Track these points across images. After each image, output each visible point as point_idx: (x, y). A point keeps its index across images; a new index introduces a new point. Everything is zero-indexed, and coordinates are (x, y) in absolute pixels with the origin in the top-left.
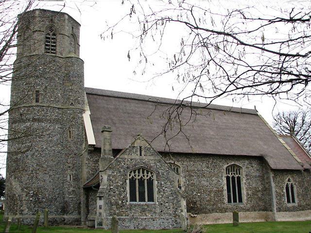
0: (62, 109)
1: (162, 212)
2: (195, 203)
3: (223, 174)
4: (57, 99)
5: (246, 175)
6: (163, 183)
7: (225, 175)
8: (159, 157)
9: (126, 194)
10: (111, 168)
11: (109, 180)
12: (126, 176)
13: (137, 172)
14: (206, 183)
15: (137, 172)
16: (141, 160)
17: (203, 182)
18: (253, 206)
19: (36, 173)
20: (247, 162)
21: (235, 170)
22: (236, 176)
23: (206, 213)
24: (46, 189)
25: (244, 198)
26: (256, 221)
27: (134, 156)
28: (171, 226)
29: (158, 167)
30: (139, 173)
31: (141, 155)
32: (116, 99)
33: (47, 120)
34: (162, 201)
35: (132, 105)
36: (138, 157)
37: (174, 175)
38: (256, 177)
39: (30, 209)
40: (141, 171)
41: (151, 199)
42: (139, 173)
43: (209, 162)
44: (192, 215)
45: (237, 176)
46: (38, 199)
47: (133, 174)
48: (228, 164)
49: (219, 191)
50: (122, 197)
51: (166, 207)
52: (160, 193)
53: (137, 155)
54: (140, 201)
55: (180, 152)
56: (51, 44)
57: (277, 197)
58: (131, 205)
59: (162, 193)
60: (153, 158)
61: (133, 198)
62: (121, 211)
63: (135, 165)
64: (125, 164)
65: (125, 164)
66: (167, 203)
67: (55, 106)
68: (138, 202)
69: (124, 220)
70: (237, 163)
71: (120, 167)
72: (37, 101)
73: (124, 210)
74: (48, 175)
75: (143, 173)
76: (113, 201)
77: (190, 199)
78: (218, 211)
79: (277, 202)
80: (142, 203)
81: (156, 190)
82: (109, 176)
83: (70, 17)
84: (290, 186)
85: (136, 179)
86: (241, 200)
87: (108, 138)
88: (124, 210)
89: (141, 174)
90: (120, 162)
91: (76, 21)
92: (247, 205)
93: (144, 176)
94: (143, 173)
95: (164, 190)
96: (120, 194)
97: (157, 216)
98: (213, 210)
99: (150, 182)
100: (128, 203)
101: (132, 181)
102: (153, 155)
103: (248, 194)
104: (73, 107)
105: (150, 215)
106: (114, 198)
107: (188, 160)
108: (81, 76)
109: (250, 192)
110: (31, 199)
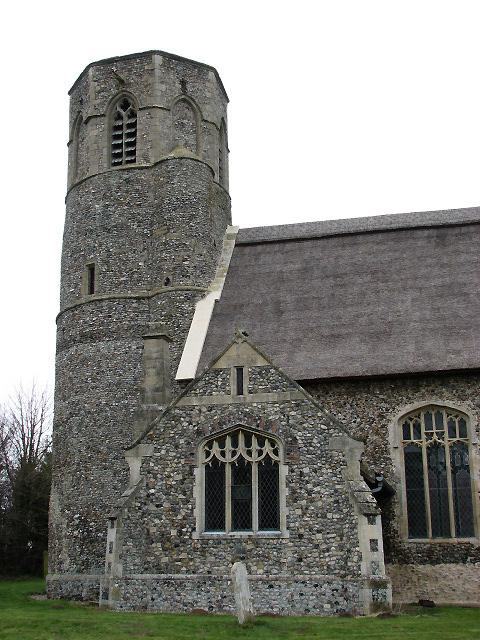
0: (149, 298)
1: (300, 560)
6: (306, 470)
8: (309, 399)
9: (192, 510)
10: (151, 438)
11: (146, 471)
13: (228, 441)
15: (228, 441)
16: (237, 406)
19: (87, 469)
24: (106, 506)
27: (218, 397)
28: (327, 606)
30: (235, 444)
31: (240, 392)
32: (320, 242)
33: (109, 334)
35: (362, 249)
36: (229, 400)
37: (344, 444)
39: (74, 560)
40: (241, 438)
41: (270, 520)
42: (235, 444)
46: (89, 532)
47: (216, 450)
50: (180, 517)
51: (317, 546)
52: (295, 500)
53: (228, 393)
54: (235, 527)
55: (456, 367)
56: (157, 135)
61: (214, 521)
62: (175, 557)
63: (220, 424)
64: (190, 423)
65: (190, 423)
66: (319, 532)
67: (130, 294)
68: (228, 532)
69: (181, 584)
72: (92, 291)
73: (183, 556)
74: (110, 472)
75: (248, 444)
76: (153, 530)
80: (238, 534)
81: (284, 492)
82: (146, 461)
83: (171, 59)
85: (223, 464)
87: (155, 355)
88: (183, 556)
89: (241, 449)
90: (177, 418)
91: (192, 62)
93: (223, 454)
94: (248, 444)
95: (309, 492)
96: (175, 510)
97: (285, 574)
99: (269, 471)
100: (195, 536)
101: (214, 472)
102: (276, 388)
104: (170, 288)
105: (261, 571)
106: (157, 521)
110: (76, 533)
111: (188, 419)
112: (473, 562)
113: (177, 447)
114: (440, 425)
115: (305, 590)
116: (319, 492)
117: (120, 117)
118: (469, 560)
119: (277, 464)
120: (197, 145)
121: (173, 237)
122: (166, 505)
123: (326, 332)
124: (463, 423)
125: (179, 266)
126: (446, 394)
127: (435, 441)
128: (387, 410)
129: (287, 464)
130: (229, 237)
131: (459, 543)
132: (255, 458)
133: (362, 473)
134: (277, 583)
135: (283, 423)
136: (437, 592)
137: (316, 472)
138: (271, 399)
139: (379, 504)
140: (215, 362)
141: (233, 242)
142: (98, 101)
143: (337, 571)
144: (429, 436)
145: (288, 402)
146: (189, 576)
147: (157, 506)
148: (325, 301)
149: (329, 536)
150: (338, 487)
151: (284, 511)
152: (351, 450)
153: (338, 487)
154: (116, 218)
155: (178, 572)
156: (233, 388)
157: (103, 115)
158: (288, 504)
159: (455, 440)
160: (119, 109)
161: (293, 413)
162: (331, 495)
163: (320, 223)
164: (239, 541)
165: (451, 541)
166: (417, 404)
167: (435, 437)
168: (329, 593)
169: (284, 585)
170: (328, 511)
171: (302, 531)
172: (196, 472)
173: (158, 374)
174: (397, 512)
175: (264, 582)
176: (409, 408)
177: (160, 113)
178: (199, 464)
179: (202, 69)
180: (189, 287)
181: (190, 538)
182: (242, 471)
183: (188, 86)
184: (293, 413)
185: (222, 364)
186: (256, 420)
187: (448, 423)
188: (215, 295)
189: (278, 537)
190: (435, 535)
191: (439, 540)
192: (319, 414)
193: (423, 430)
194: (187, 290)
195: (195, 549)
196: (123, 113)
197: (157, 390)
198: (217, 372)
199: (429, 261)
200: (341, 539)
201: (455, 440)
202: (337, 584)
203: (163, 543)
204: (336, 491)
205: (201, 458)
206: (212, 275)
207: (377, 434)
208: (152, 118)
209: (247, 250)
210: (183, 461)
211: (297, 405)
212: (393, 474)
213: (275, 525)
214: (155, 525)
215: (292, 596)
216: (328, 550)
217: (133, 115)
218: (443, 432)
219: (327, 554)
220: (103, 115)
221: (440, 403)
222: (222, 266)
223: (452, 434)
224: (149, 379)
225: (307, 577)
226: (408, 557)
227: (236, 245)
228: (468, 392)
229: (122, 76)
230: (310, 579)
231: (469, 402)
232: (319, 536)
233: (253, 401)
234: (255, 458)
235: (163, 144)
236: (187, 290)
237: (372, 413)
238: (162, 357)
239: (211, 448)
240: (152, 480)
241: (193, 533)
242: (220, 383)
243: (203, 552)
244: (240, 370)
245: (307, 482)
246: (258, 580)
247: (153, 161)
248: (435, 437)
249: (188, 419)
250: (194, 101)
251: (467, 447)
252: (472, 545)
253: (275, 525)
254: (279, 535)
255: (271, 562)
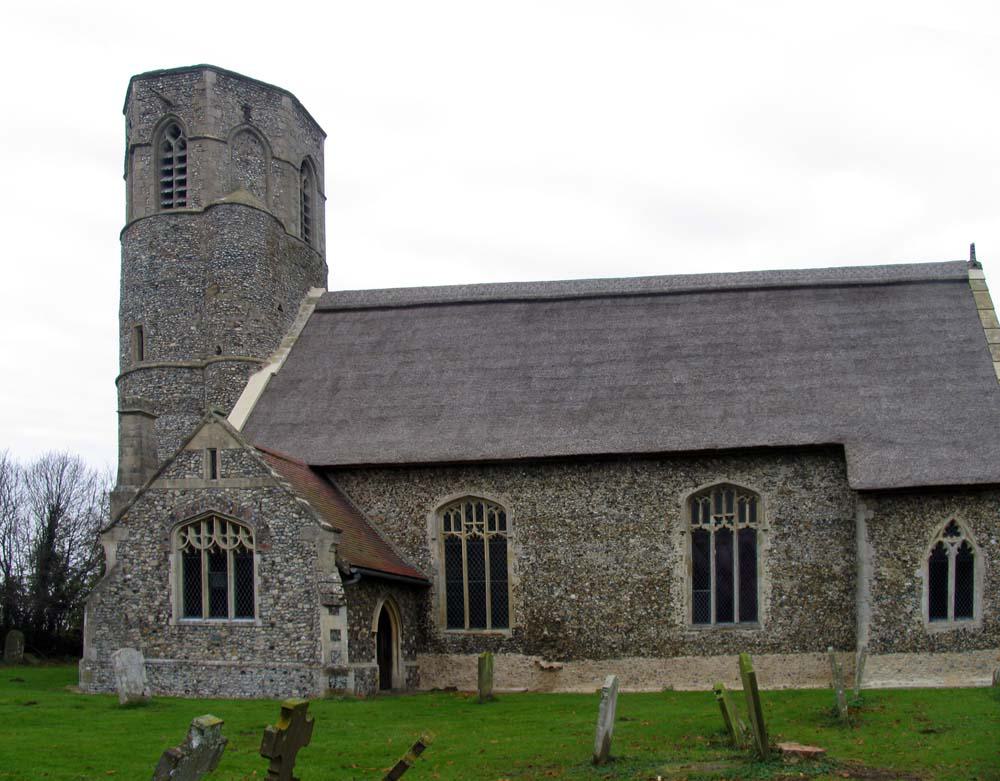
1: (272, 648)
2: (558, 626)
3: (674, 523)
4: (187, 341)
5: (779, 522)
6: (278, 560)
7: (682, 524)
9: (168, 596)
12: (167, 544)
13: (204, 527)
14: (600, 559)
15: (204, 527)
16: (210, 490)
17: (589, 555)
18: (798, 633)
20: (785, 471)
21: (735, 505)
22: (736, 527)
23: (596, 656)
25: (764, 605)
26: (804, 687)
29: (264, 509)
30: (211, 530)
31: (214, 476)
34: (276, 615)
35: (343, 327)
38: (820, 525)
41: (245, 608)
42: (211, 530)
43: (618, 483)
44: (544, 664)
45: (742, 526)
47: (192, 535)
48: (696, 486)
49: (651, 584)
51: (287, 635)
52: (267, 589)
53: (201, 476)
54: (213, 615)
57: (878, 599)
58: (181, 627)
59: (276, 592)
60: (248, 484)
61: (192, 608)
62: (153, 642)
64: (164, 507)
66: (290, 621)
67: (181, 362)
70: (740, 480)
71: (150, 517)
73: (161, 641)
75: (224, 531)
77: (540, 611)
78: (643, 650)
79: (876, 619)
80: (213, 621)
81: (258, 581)
82: (122, 544)
83: (227, 77)
84: (952, 554)
86: (750, 613)
87: (132, 433)
89: (217, 536)
92: (769, 629)
94: (224, 531)
95: (281, 582)
96: (151, 596)
98: (625, 649)
99: (244, 560)
100: (172, 622)
101: (191, 560)
102: (249, 473)
103: (778, 590)
105: (235, 658)
106: (134, 607)
107: (536, 483)
108: (965, 262)
109: (787, 585)
111: (161, 503)
112: (504, 652)
113: (152, 532)
114: (480, 518)
115: (275, 676)
116: (290, 582)
117: (170, 148)
118: (500, 650)
119: (251, 552)
120: (267, 189)
121: (224, 299)
122: (143, 591)
123: (374, 413)
124: (502, 517)
125: (231, 332)
126: (485, 485)
127: (724, 526)
128: (426, 500)
129: (259, 552)
130: (310, 301)
131: (493, 634)
132: (204, 546)
133: (337, 564)
134: (249, 669)
135: (257, 510)
136: (469, 679)
137: (287, 561)
138: (243, 486)
139: (347, 595)
140: (187, 441)
141: (313, 307)
142: (143, 126)
143: (306, 659)
144: (469, 528)
145: (260, 488)
146: (166, 661)
147: (135, 592)
148: (385, 381)
149: (300, 625)
150: (307, 577)
151: (257, 599)
152: (321, 541)
153: (307, 577)
154: (163, 274)
155: (157, 656)
156: (206, 471)
157: (148, 145)
158: (261, 594)
159: (494, 532)
160: (168, 138)
161: (265, 500)
162: (300, 586)
163: (410, 290)
164: (214, 628)
165: (486, 632)
166: (456, 495)
167: (475, 529)
168: (297, 680)
169: (255, 671)
170: (299, 601)
171: (273, 620)
172: (172, 558)
173: (136, 453)
174: (433, 603)
175: (236, 668)
176: (447, 498)
177: (212, 146)
178: (174, 550)
179: (272, 93)
180: (241, 358)
181: (167, 624)
182: (218, 559)
183: (255, 115)
184: (265, 500)
185: (194, 445)
186: (229, 507)
187: (489, 515)
188: (274, 367)
189: (251, 625)
190: (472, 625)
191: (476, 631)
192: (291, 502)
193: (464, 522)
194: (239, 361)
195: (173, 635)
196: (173, 142)
197: (135, 471)
198: (190, 453)
199: (508, 339)
200: (311, 629)
201: (494, 532)
202: (305, 671)
203: (141, 628)
204: (307, 581)
205: (176, 544)
206: (277, 344)
207: (416, 524)
208: (203, 151)
209: (326, 317)
210: (158, 547)
211: (270, 492)
212: (430, 565)
213: (251, 615)
214: (133, 611)
215: (263, 681)
216: (298, 639)
217: (184, 147)
218: (483, 525)
219: (297, 643)
220: (148, 145)
221: (478, 494)
222: (291, 334)
223: (492, 527)
224: (127, 458)
225: (278, 664)
226: (444, 647)
227: (315, 311)
228: (508, 483)
229: (168, 96)
230: (280, 666)
231: (507, 494)
232: (290, 625)
233: (225, 486)
234: (204, 546)
235: (218, 184)
236: (239, 361)
237: (412, 503)
238: (140, 435)
239: (187, 533)
240: (129, 565)
241: (170, 620)
242: (192, 466)
243: (181, 637)
244: (213, 452)
245: (279, 572)
246: (230, 667)
247: (205, 204)
248: (724, 522)
249: (161, 503)
250: (260, 132)
251: (506, 540)
252: (504, 637)
253: (251, 615)
254: (252, 623)
255: (244, 649)
